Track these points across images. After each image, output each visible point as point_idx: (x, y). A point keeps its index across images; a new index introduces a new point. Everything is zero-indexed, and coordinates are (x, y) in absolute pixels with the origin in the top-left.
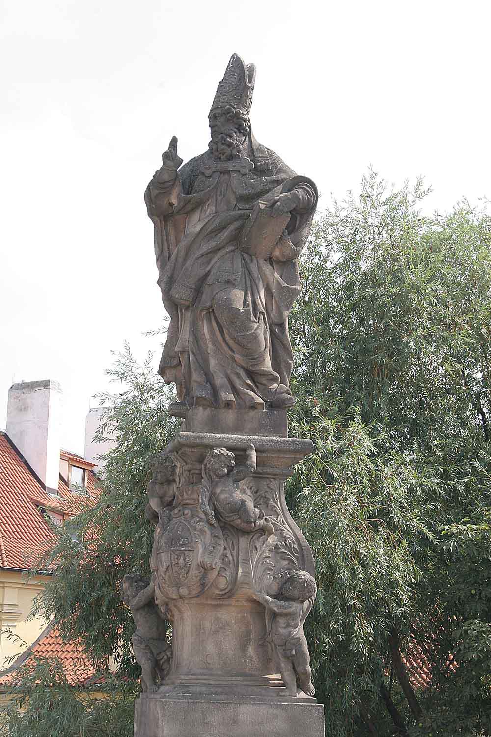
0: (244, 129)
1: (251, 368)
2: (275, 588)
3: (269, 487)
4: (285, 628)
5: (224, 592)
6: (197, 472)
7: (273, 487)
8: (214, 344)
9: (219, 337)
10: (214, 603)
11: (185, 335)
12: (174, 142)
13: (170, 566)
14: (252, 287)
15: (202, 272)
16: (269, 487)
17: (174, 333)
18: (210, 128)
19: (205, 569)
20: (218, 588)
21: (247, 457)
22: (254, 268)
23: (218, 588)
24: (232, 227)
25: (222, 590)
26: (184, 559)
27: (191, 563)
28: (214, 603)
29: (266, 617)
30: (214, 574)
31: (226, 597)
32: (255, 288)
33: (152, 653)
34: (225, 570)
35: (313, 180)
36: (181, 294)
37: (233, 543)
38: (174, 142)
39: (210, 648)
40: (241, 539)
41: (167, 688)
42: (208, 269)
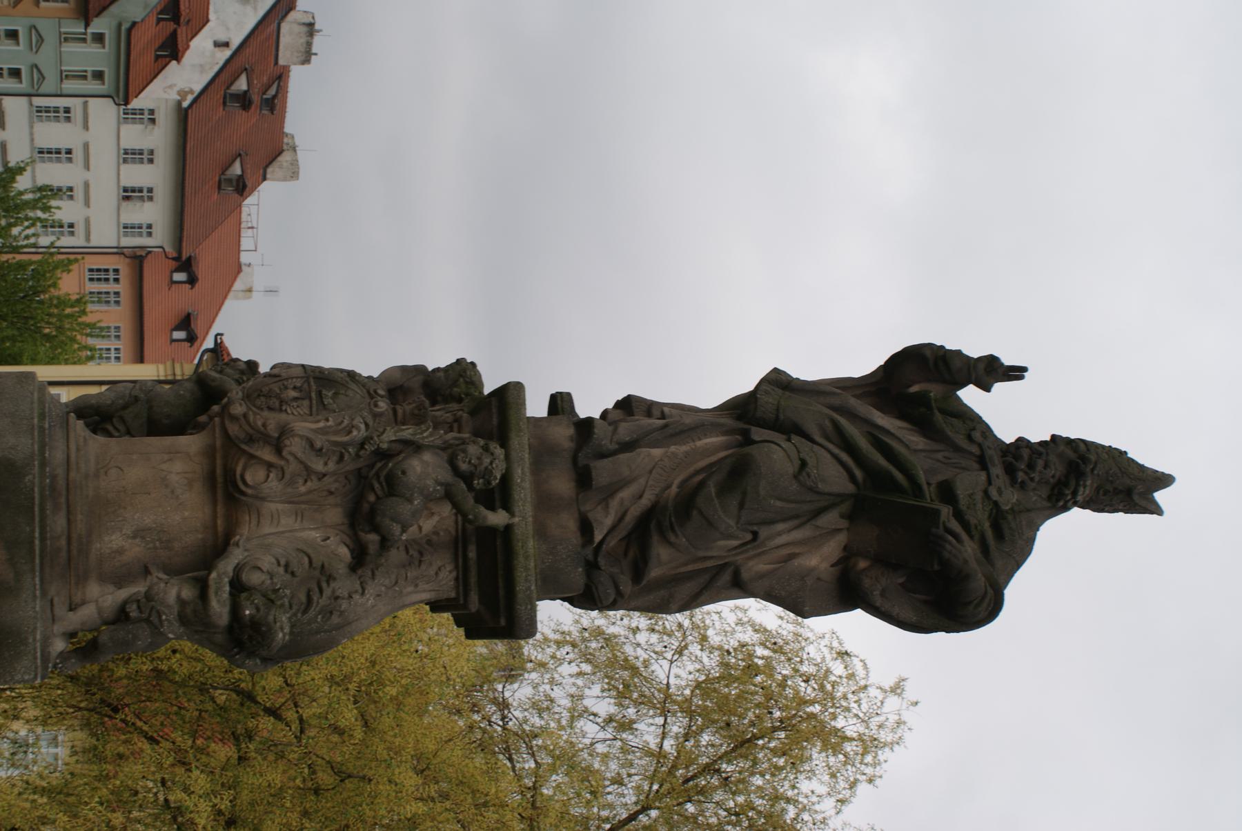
0: (1058, 503)
4: (179, 597)
7: (441, 575)
8: (687, 454)
10: (219, 471)
12: (1016, 373)
13: (278, 379)
18: (1048, 438)
20: (244, 469)
21: (492, 508)
22: (831, 519)
26: (296, 399)
28: (219, 471)
30: (267, 454)
32: (796, 522)
33: (125, 407)
35: (1002, 614)
38: (1016, 373)
40: (339, 510)
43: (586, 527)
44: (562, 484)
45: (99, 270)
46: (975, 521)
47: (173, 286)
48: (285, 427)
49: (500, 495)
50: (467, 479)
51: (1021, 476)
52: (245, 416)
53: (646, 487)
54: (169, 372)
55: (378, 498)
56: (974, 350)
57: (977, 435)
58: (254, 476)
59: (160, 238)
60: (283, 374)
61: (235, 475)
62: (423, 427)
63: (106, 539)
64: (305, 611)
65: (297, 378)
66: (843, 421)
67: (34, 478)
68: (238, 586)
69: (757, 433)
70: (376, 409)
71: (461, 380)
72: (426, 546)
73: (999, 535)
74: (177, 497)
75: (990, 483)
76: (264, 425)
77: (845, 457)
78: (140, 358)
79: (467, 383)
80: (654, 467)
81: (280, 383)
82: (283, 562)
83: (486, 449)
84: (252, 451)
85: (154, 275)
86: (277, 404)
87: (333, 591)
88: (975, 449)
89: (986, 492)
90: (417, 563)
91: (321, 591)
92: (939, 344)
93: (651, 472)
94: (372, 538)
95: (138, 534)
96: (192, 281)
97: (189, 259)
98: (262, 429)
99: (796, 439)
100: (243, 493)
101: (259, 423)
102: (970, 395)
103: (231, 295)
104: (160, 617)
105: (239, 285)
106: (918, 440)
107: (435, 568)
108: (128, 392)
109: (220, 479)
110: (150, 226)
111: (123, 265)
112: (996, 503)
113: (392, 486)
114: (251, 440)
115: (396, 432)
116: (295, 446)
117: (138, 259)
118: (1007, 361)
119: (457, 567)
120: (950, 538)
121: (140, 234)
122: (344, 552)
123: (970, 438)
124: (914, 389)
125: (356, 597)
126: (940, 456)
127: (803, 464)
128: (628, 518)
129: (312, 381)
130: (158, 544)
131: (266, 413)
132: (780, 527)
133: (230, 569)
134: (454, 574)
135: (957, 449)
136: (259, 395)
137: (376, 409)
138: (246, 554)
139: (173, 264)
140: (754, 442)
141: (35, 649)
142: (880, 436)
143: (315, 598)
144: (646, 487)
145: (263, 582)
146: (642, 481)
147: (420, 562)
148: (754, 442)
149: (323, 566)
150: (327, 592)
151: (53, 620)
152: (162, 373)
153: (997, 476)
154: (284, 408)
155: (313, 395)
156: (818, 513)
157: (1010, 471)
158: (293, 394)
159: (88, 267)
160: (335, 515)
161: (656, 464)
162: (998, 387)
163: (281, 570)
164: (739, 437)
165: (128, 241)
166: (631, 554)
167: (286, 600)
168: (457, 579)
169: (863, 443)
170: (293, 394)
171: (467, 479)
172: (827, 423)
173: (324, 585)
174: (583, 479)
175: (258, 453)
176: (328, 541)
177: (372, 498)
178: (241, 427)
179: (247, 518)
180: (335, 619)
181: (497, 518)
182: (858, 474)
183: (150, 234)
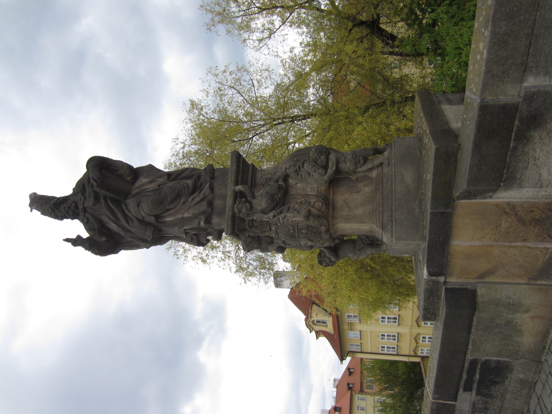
0: (65, 199)
1: (190, 191)
2: (321, 171)
3: (261, 178)
4: (346, 164)
5: (324, 203)
6: (251, 222)
7: (261, 176)
9: (172, 211)
10: (331, 210)
11: (175, 231)
12: (67, 240)
13: (308, 238)
14: (145, 192)
15: (136, 222)
16: (261, 178)
17: (178, 238)
19: (309, 215)
21: (241, 192)
23: (322, 207)
24: (111, 205)
25: (323, 205)
27: (305, 225)
28: (331, 210)
29: (338, 177)
30: (314, 211)
31: (327, 202)
32: (146, 190)
33: (363, 248)
34: (310, 202)
36: (149, 234)
37: (293, 199)
38: (67, 240)
39: (360, 211)
41: (457, 29)
42: (134, 218)
43: (212, 189)
44: (218, 203)
45: (371, 389)
46: (89, 188)
47: (353, 383)
48: (307, 220)
49: (238, 195)
50: (247, 201)
51: (73, 205)
52: (321, 226)
53: (191, 202)
54: (354, 355)
55: (277, 194)
56: (80, 249)
57: (85, 221)
58: (319, 204)
59: (357, 396)
60: (307, 240)
61: (325, 206)
62: (260, 220)
63: (370, 190)
64: (305, 161)
65: (302, 238)
66: (126, 225)
67: (395, 204)
68: (325, 167)
69: (152, 220)
70: (276, 227)
71: (248, 243)
72: (264, 184)
73: (84, 186)
74: (345, 203)
75: (84, 203)
76: (314, 221)
77: (127, 212)
78: (362, 359)
79: (246, 242)
80: (188, 209)
81: (308, 236)
82: (311, 176)
83: (240, 212)
84: (319, 213)
85: (357, 387)
86: (309, 228)
87: (295, 167)
88: (87, 215)
89: (85, 199)
90: (268, 179)
91: (299, 167)
92: (93, 254)
93: (189, 208)
94: (281, 183)
95: (359, 192)
96: (348, 384)
97: (349, 390)
98: (315, 219)
99: (141, 218)
100: (323, 199)
101: (316, 222)
102: (85, 235)
103: (339, 380)
104: (352, 157)
105: (337, 383)
106: (105, 219)
107: (262, 178)
108: (362, 253)
109: (331, 207)
110: (358, 399)
111: (366, 390)
112: (83, 195)
113: (272, 197)
114: (319, 217)
115: (269, 216)
116: (304, 211)
117: (362, 391)
118: (70, 244)
119: (255, 179)
120: (95, 178)
121: (361, 398)
122: (291, 181)
123: (88, 219)
124: (104, 239)
125: (288, 167)
126: (98, 213)
127: (138, 205)
128: (197, 192)
129: (297, 237)
130: (353, 188)
131: (313, 226)
132: (151, 189)
133: (328, 171)
134: (256, 176)
135: (92, 215)
136: (316, 233)
137: (276, 227)
138: (323, 178)
139: (353, 389)
140: (155, 216)
141: (394, 148)
142: (114, 219)
143: (301, 164)
144: (191, 202)
145: (318, 169)
146: (192, 204)
147: (267, 179)
148: (155, 216)
149: (298, 175)
150: (297, 167)
151: (388, 158)
152: (356, 355)
153: (81, 205)
154: (307, 226)
155: (296, 231)
156: (138, 194)
157: (77, 207)
158: (304, 231)
159: (374, 390)
160: (292, 192)
161: (187, 211)
162: (74, 237)
163: (312, 174)
164: (160, 220)
165: (364, 396)
166: (200, 183)
167: (311, 164)
168: (256, 174)
169: (120, 216)
170: (304, 231)
171: (247, 201)
172: (130, 224)
173: (298, 169)
174: (210, 204)
175: (317, 211)
176: (295, 183)
177: (279, 195)
178: (323, 222)
179: (322, 191)
180: (295, 159)
181: (239, 188)
182: (124, 207)
183: (358, 397)
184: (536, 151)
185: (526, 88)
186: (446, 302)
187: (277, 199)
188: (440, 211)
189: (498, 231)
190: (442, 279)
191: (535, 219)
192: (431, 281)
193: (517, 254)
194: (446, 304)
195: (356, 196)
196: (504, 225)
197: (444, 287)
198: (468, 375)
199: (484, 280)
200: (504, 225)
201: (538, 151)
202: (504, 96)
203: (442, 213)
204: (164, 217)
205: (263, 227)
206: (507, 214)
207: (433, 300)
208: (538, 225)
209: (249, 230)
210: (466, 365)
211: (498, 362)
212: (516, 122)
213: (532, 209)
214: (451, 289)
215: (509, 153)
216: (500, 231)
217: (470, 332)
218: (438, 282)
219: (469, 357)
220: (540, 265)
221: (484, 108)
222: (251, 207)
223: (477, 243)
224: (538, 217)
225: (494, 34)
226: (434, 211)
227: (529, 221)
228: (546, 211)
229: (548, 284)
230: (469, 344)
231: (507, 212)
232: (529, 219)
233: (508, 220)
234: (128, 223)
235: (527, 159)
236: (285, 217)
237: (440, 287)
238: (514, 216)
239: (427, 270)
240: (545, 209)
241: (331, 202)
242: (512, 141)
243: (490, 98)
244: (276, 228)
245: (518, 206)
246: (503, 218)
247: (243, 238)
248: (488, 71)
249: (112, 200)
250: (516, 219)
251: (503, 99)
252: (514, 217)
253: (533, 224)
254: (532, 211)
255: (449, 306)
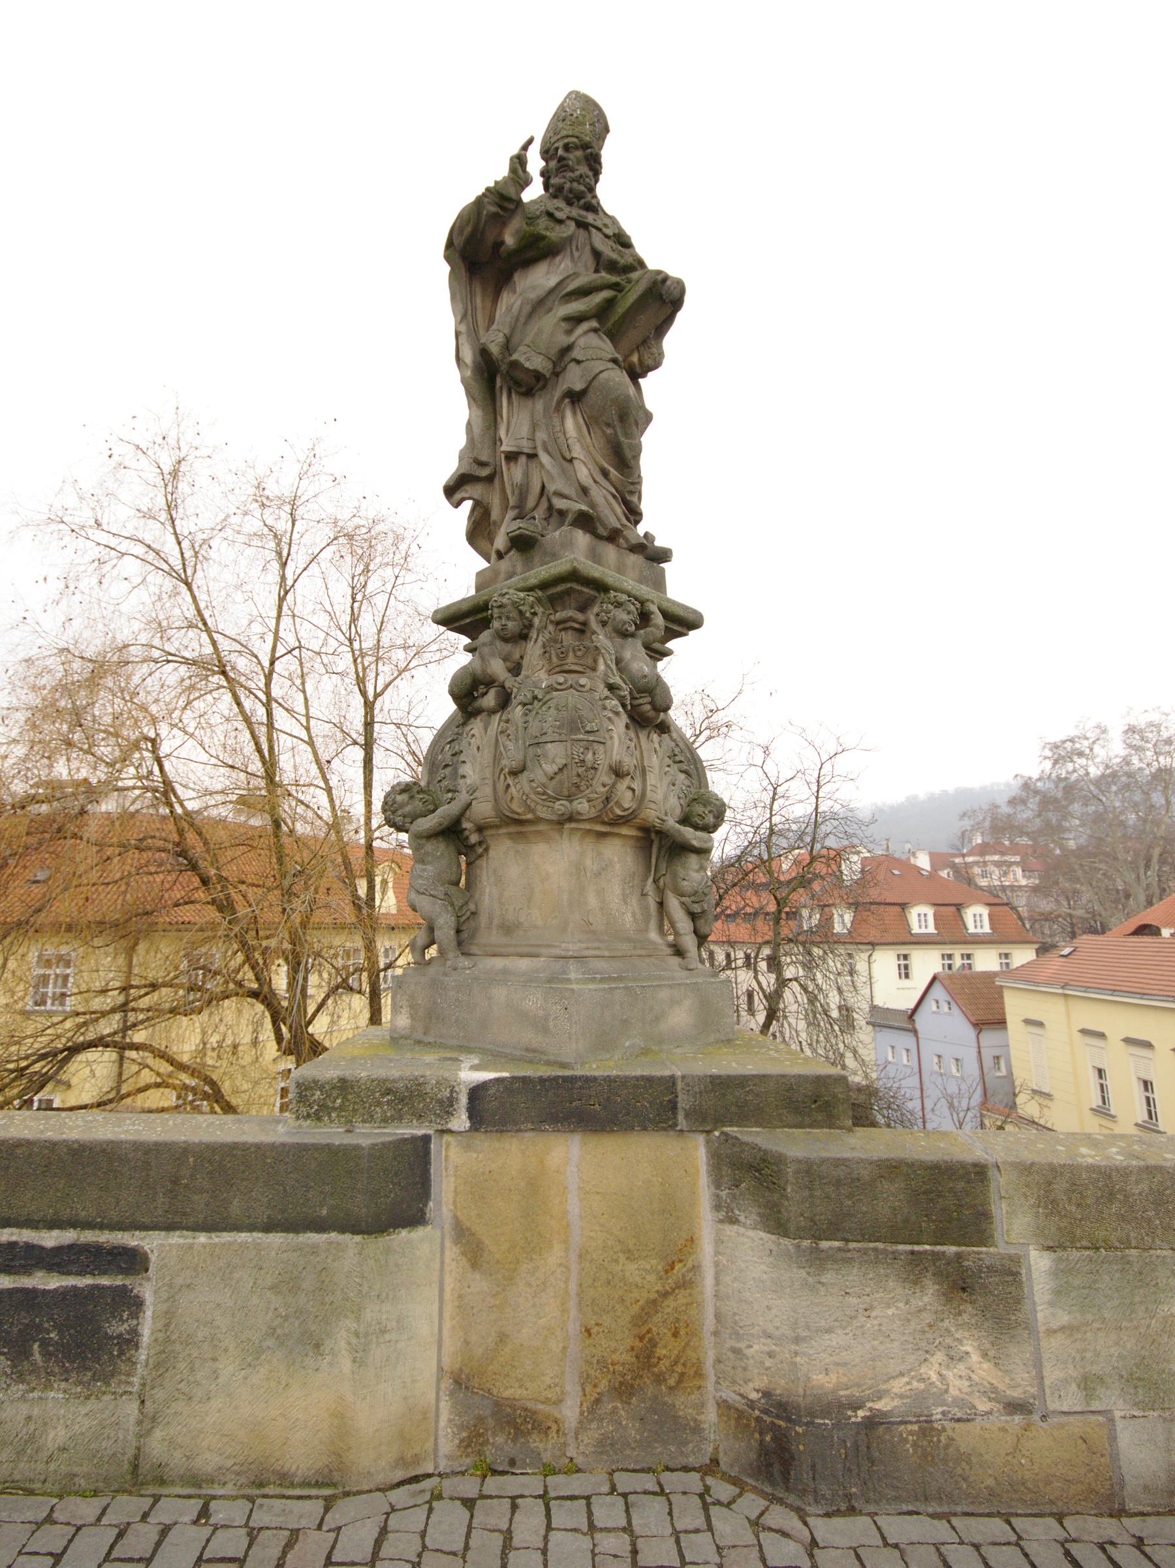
33: (452, 905)
39: (592, 901)
42: (572, 339)
44: (610, 552)
68: (685, 820)
124: (510, 240)
126: (576, 254)
140: (584, 392)
158: (589, 756)
184: (888, 1306)
185: (1027, 1256)
186: (390, 1142)
187: (641, 701)
188: (680, 1099)
189: (615, 1257)
190: (461, 1121)
191: (655, 1346)
192: (452, 1091)
193: (542, 1321)
194: (383, 1144)
195: (618, 891)
196: (632, 1270)
197: (431, 1132)
198: (58, 1250)
199: (448, 1244)
200: (632, 1270)
201: (890, 1312)
202: (1007, 1213)
203: (673, 1106)
204: (574, 413)
205: (579, 653)
206: (666, 1272)
207: (379, 1104)
208: (637, 1357)
209: (552, 617)
210: (130, 1239)
211: (131, 1341)
212: (952, 1249)
213: (682, 1332)
214: (427, 1153)
215: (880, 1245)
216: (616, 1261)
217: (268, 1228)
218: (450, 1114)
219: (149, 1242)
220: (507, 1393)
221: (979, 1173)
222: (625, 635)
223: (574, 1206)
224: (660, 1351)
225: (1124, 1173)
226: (680, 1085)
227: (649, 1331)
228: (679, 1368)
229: (440, 1433)
230: (213, 1235)
231: (673, 1269)
232: (654, 1329)
233: (648, 1277)
234: (567, 319)
235: (868, 1290)
236: (617, 713)
237: (431, 1122)
238: (661, 1289)
239: (490, 1080)
240: (684, 1365)
241: (616, 830)
242: (908, 1247)
243: (1000, 1182)
244: (583, 686)
245: (690, 1295)
246: (654, 1262)
247: (531, 599)
248: (1055, 1171)
249: (610, 303)
250: (653, 1296)
251: (999, 1210)
252: (658, 1292)
253: (640, 1345)
254: (675, 1334)
255: (378, 1152)
